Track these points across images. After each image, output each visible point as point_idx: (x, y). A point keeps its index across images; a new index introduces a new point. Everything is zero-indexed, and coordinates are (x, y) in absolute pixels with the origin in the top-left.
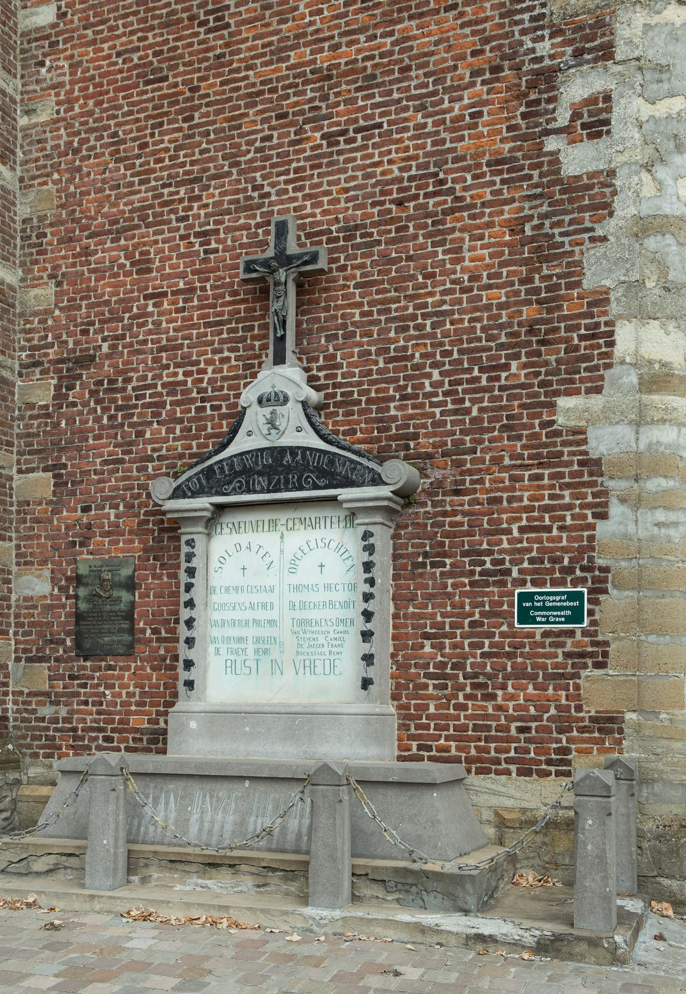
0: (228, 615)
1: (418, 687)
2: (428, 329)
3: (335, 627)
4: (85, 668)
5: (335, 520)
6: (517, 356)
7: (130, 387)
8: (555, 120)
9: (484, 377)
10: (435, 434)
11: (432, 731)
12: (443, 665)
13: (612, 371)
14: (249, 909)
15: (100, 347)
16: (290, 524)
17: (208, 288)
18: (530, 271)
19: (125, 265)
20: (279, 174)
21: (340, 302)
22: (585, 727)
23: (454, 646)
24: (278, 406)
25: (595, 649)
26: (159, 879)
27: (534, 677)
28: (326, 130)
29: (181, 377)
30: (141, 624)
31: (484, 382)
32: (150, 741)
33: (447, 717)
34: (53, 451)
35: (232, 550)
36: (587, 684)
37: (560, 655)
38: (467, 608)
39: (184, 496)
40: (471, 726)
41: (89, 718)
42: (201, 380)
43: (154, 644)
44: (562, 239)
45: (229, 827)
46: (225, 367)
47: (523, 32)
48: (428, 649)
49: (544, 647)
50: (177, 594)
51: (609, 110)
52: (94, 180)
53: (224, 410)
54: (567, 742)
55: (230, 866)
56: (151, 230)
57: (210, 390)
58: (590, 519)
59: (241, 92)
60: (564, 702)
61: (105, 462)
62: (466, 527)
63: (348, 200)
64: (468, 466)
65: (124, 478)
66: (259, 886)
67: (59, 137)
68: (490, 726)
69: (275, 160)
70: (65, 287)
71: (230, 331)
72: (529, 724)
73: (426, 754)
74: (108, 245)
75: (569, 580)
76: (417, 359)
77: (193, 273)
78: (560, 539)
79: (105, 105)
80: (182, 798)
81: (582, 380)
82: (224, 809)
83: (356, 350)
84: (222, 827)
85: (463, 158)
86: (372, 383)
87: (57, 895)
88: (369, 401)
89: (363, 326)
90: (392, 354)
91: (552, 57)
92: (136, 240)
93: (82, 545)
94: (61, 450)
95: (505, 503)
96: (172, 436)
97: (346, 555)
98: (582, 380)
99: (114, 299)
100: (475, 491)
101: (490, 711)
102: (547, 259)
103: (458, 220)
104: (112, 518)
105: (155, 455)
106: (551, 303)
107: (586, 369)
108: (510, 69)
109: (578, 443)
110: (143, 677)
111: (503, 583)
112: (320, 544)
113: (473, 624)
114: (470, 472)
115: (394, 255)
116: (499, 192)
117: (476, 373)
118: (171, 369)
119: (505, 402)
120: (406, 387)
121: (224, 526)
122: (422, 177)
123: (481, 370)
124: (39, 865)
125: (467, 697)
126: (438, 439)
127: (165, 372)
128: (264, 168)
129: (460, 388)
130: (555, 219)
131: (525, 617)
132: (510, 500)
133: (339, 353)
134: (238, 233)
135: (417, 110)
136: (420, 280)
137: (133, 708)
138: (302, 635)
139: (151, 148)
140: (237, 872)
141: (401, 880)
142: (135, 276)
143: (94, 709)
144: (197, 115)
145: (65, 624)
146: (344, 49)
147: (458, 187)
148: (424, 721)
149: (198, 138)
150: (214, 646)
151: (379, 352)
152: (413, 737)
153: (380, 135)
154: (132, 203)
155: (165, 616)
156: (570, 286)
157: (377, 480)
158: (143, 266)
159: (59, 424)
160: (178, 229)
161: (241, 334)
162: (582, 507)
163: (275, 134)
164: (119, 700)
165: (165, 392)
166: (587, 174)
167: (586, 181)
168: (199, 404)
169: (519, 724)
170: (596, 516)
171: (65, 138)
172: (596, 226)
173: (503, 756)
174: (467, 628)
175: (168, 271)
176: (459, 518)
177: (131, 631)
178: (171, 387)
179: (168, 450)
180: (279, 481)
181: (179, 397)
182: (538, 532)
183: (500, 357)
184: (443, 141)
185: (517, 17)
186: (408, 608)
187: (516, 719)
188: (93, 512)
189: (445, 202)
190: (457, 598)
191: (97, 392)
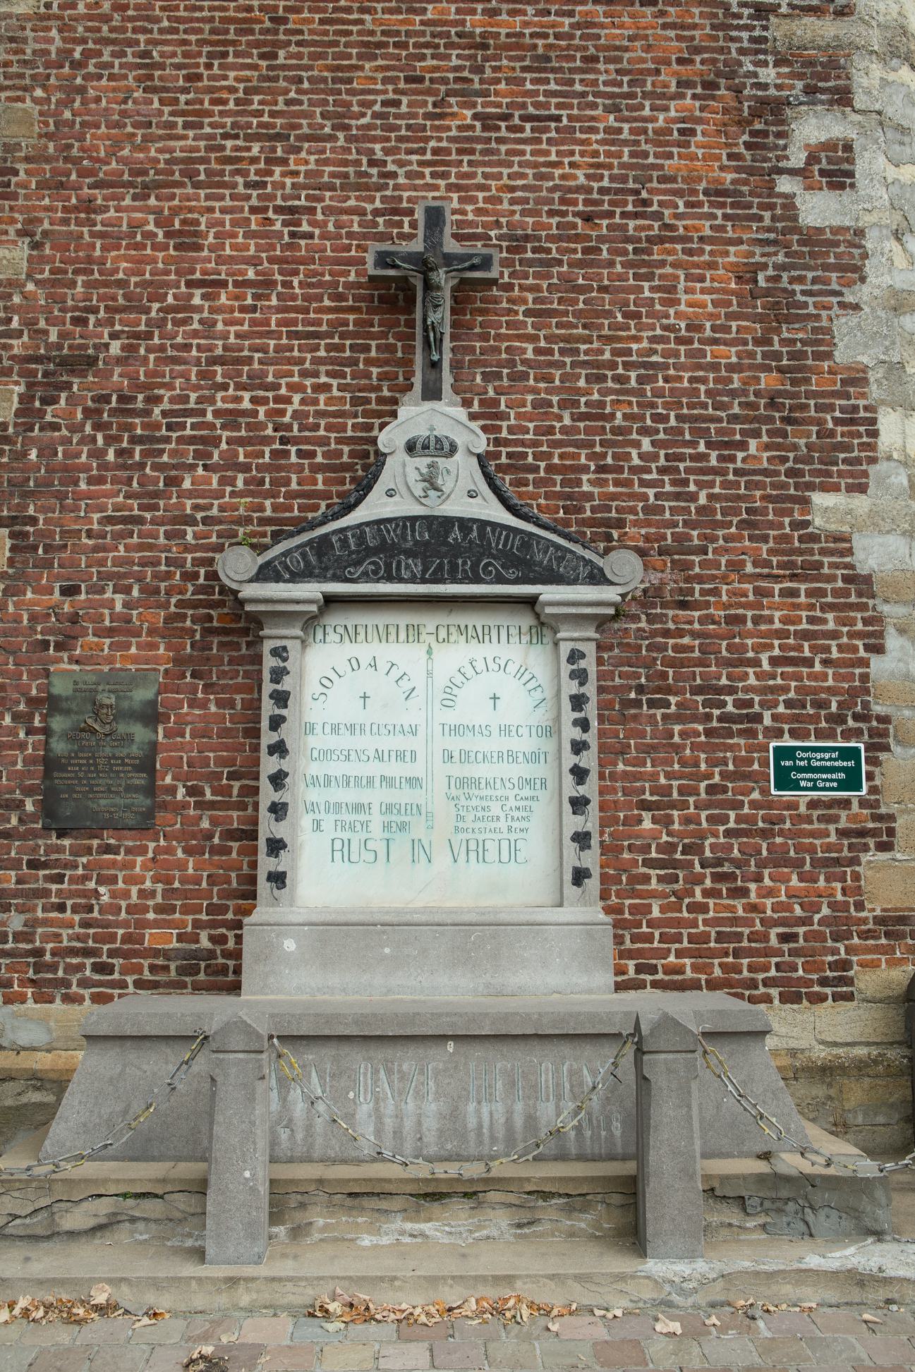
0: (337, 769)
1: (634, 879)
2: (633, 383)
3: (516, 791)
4: (60, 849)
5: (514, 631)
6: (757, 434)
7: (157, 411)
8: (788, 158)
9: (714, 455)
10: (648, 524)
11: (656, 945)
12: (671, 847)
13: (878, 467)
14: (552, 1277)
15: (107, 346)
16: (443, 634)
17: (296, 283)
18: (767, 330)
19: (156, 235)
20: (410, 152)
21: (503, 331)
22: (869, 931)
23: (687, 820)
24: (435, 457)
25: (878, 825)
26: (326, 1228)
27: (798, 864)
28: (479, 109)
29: (246, 405)
30: (168, 780)
31: (714, 462)
32: (181, 971)
33: (679, 923)
34: (12, 494)
35: (343, 667)
36: (869, 873)
37: (833, 833)
38: (703, 766)
39: (278, 578)
40: (713, 935)
41: (65, 933)
42: (282, 413)
43: (192, 812)
44: (803, 299)
45: (431, 1125)
46: (322, 397)
47: (742, 51)
48: (647, 824)
49: (811, 822)
50: (255, 733)
51: (851, 161)
52: (106, 109)
53: (319, 459)
54: (847, 953)
55: (465, 1195)
56: (202, 193)
57: (296, 427)
58: (862, 653)
59: (352, 38)
60: (839, 897)
61: (109, 520)
62: (697, 654)
63: (513, 202)
64: (697, 570)
65: (141, 547)
66: (519, 1226)
67: (50, 41)
68: (741, 934)
69: (403, 132)
70: (47, 252)
71: (329, 348)
72: (795, 930)
73: (649, 978)
74: (127, 202)
75: (839, 730)
76: (619, 419)
77: (271, 260)
78: (824, 677)
79: (130, 13)
80: (333, 1076)
81: (840, 474)
82: (417, 1092)
83: (530, 398)
84: (419, 1123)
85: (673, 179)
86: (555, 444)
87: (156, 1284)
88: (550, 469)
89: (539, 367)
90: (583, 409)
91: (779, 87)
92: (176, 202)
93: (59, 647)
94: (26, 495)
95: (750, 624)
96: (228, 489)
97: (533, 684)
98: (840, 474)
99: (133, 279)
100: (707, 605)
101: (740, 912)
102: (789, 319)
103: (669, 253)
104: (119, 607)
105: (199, 516)
106: (796, 372)
107: (845, 461)
108: (728, 89)
109: (842, 553)
110: (169, 866)
111: (752, 734)
112: (491, 665)
113: (711, 789)
114: (700, 579)
115: (580, 281)
116: (722, 228)
117: (702, 448)
118: (231, 391)
119: (742, 491)
120: (604, 455)
121: (329, 630)
122: (618, 191)
123: (709, 445)
124: (75, 1219)
125: (707, 893)
126: (653, 530)
127: (219, 395)
128: (388, 139)
129: (682, 466)
130: (795, 273)
131: (784, 781)
132: (757, 620)
133: (503, 399)
134: (345, 217)
135: (608, 110)
136: (620, 319)
137: (151, 916)
138: (463, 802)
139: (206, 83)
140: (480, 1204)
141: (769, 1194)
142: (172, 252)
143: (77, 918)
144: (282, 53)
145: (22, 775)
146: (504, 17)
147: (667, 212)
148: (645, 929)
149: (282, 84)
150: (311, 816)
151: (563, 405)
152: (630, 954)
153: (557, 130)
154: (171, 151)
155: (212, 767)
156: (819, 356)
157: (597, 577)
158: (188, 240)
159: (25, 454)
160: (249, 197)
161: (348, 354)
162: (851, 635)
163: (405, 100)
164: (123, 904)
165: (218, 423)
166: (831, 228)
167: (829, 235)
168: (277, 446)
169: (780, 930)
170: (868, 648)
171: (58, 43)
172: (845, 290)
173: (761, 976)
174: (703, 795)
175: (228, 252)
176: (686, 640)
177: (151, 790)
178: (231, 418)
179: (222, 509)
180: (441, 566)
181: (243, 433)
182: (796, 665)
183: (733, 432)
184: (645, 155)
185: (734, 33)
186: (616, 765)
187: (777, 923)
188: (83, 597)
189: (650, 228)
190: (688, 751)
191: (99, 412)
